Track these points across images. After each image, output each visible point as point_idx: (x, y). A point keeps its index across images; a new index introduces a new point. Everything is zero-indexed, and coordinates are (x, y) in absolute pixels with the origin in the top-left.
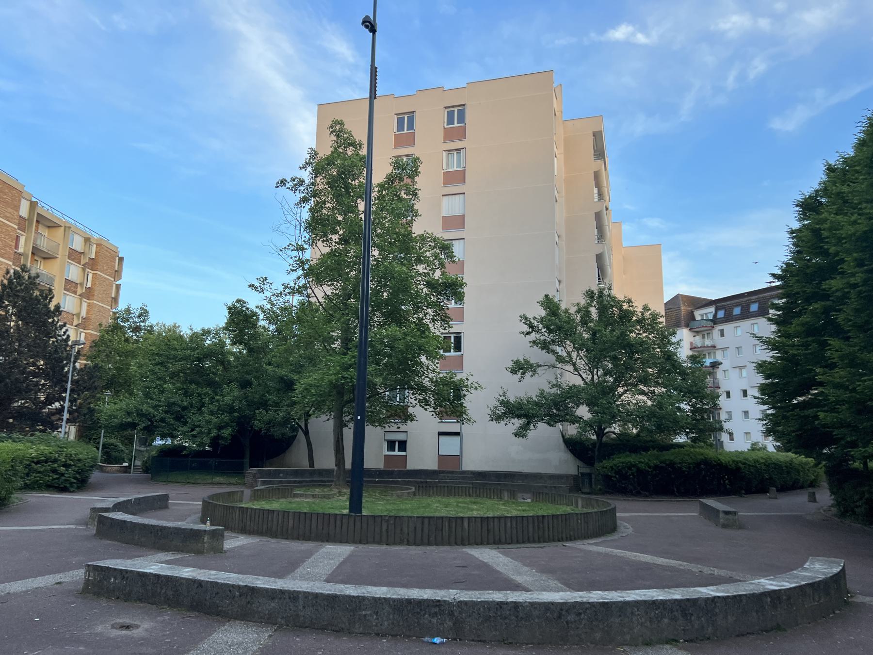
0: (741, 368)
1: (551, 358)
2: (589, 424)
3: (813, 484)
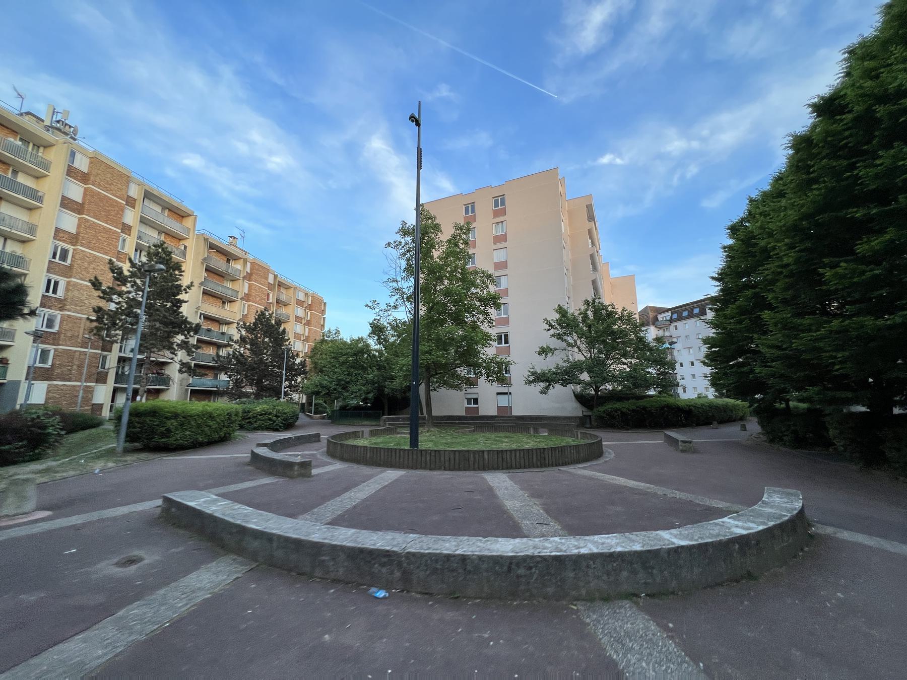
0: (689, 348)
1: (564, 344)
2: (589, 384)
3: (742, 419)
